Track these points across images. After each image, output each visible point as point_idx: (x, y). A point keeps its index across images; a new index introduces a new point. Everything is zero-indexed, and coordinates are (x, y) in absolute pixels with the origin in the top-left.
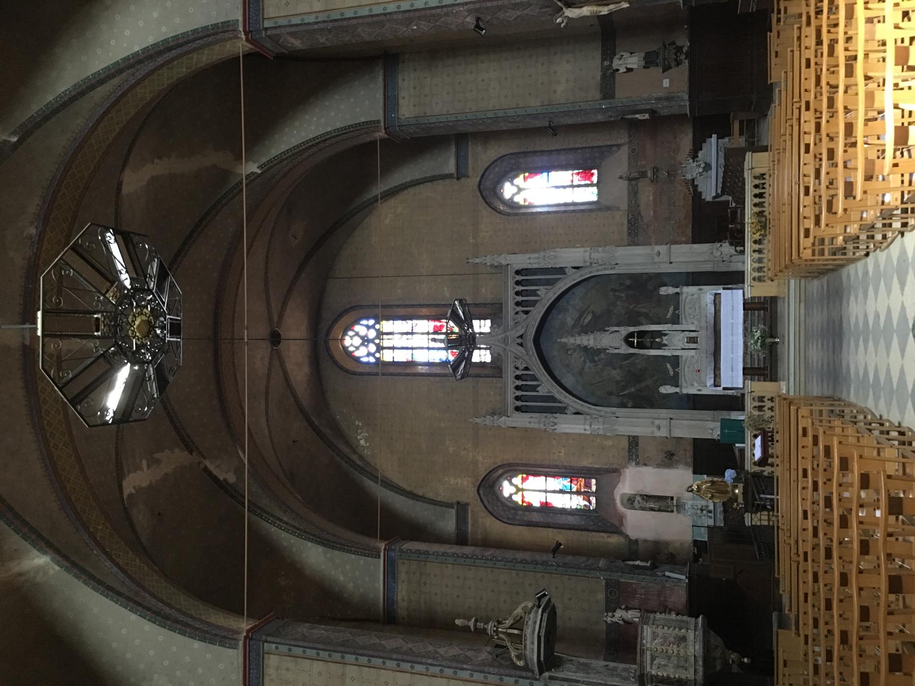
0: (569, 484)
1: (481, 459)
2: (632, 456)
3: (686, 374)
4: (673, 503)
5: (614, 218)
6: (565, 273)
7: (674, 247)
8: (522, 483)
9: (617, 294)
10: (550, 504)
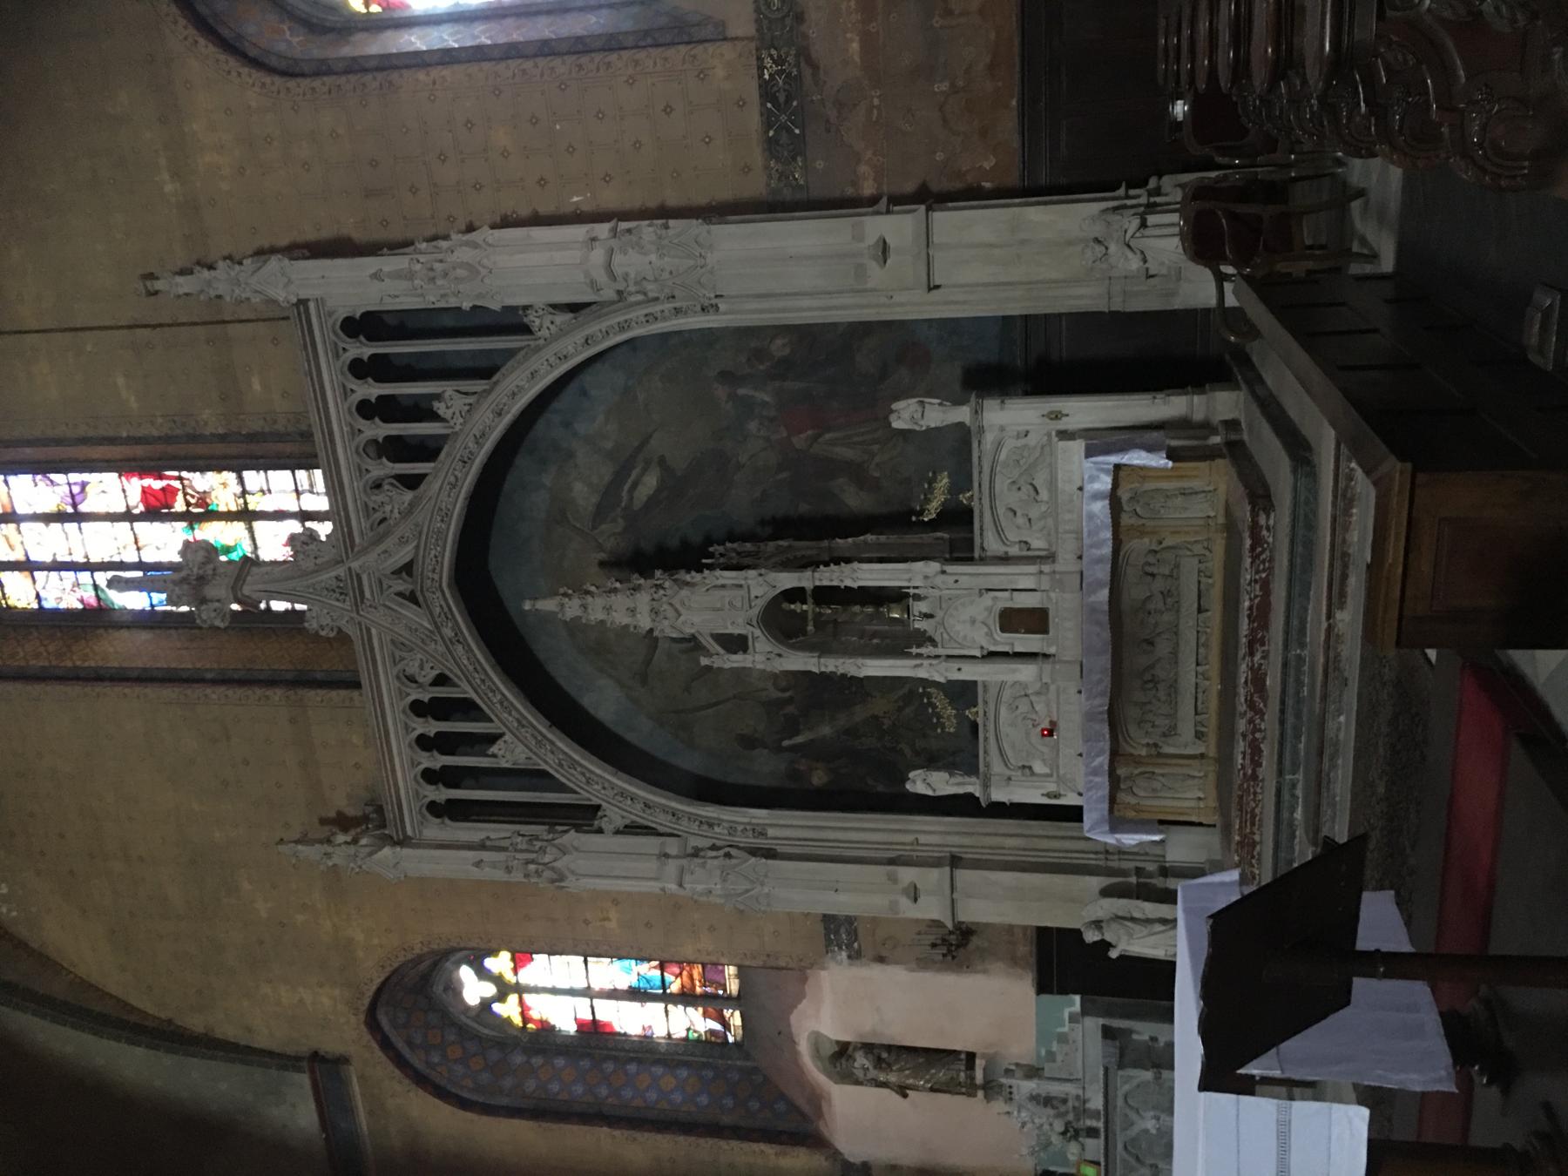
0: (658, 972)
1: (360, 937)
2: (837, 933)
3: (1005, 729)
4: (973, 1078)
5: (702, 75)
6: (526, 330)
7: (946, 221)
8: (515, 971)
9: (741, 391)
10: (608, 1025)
